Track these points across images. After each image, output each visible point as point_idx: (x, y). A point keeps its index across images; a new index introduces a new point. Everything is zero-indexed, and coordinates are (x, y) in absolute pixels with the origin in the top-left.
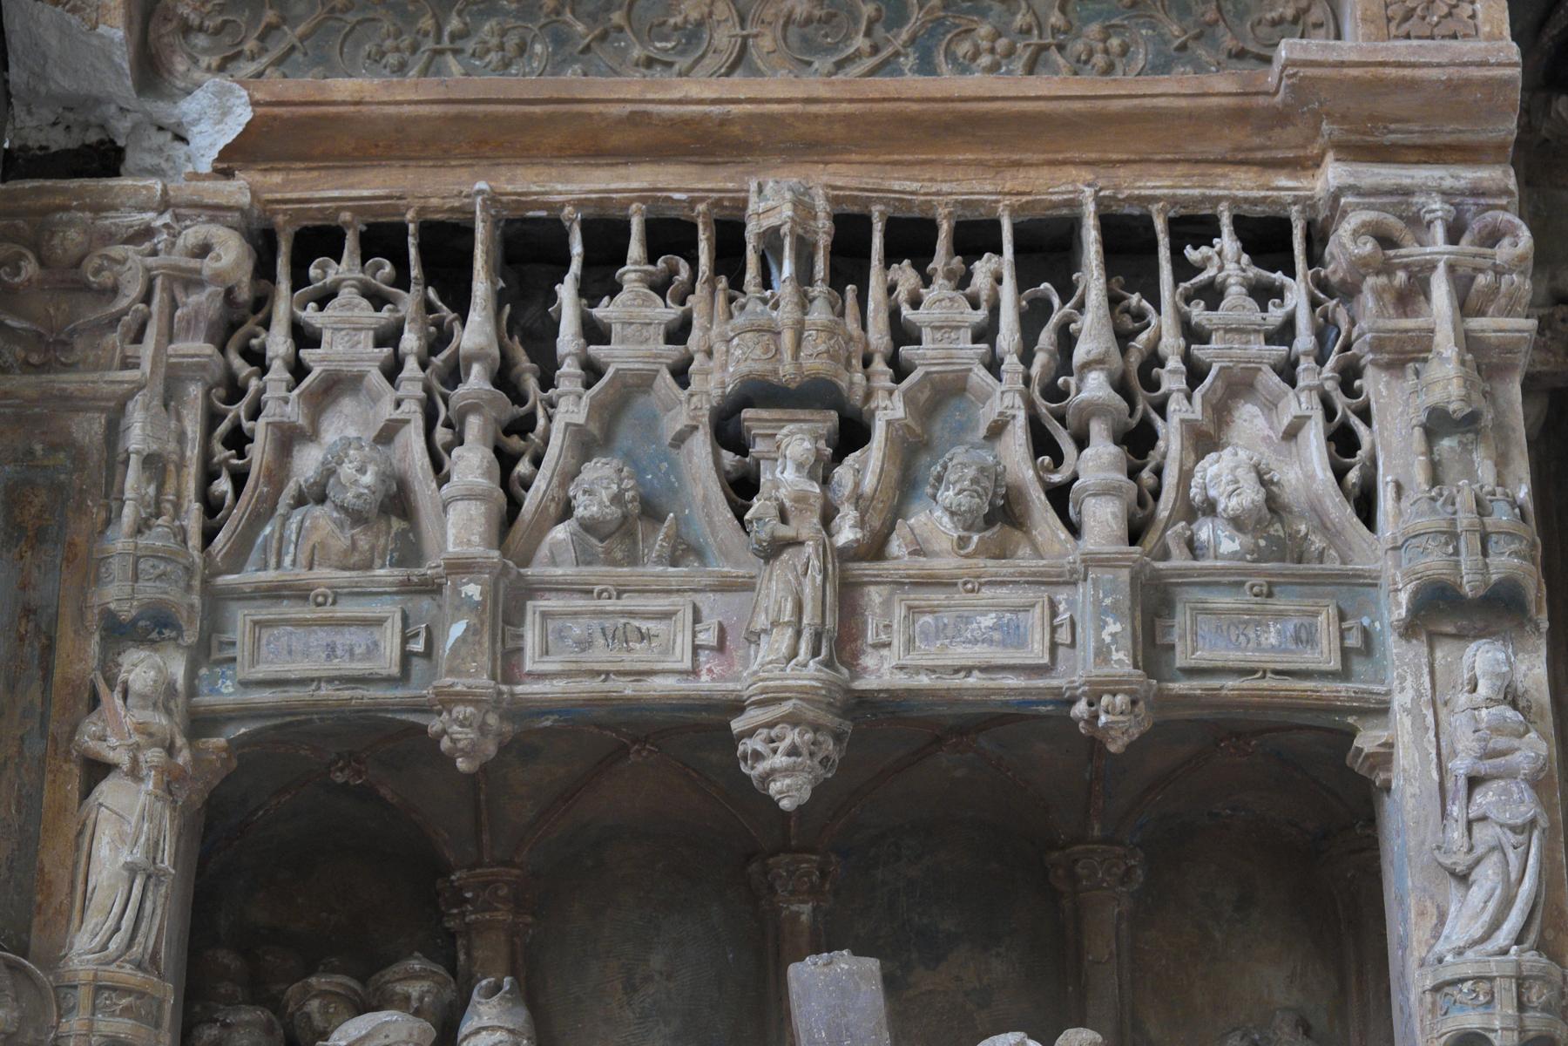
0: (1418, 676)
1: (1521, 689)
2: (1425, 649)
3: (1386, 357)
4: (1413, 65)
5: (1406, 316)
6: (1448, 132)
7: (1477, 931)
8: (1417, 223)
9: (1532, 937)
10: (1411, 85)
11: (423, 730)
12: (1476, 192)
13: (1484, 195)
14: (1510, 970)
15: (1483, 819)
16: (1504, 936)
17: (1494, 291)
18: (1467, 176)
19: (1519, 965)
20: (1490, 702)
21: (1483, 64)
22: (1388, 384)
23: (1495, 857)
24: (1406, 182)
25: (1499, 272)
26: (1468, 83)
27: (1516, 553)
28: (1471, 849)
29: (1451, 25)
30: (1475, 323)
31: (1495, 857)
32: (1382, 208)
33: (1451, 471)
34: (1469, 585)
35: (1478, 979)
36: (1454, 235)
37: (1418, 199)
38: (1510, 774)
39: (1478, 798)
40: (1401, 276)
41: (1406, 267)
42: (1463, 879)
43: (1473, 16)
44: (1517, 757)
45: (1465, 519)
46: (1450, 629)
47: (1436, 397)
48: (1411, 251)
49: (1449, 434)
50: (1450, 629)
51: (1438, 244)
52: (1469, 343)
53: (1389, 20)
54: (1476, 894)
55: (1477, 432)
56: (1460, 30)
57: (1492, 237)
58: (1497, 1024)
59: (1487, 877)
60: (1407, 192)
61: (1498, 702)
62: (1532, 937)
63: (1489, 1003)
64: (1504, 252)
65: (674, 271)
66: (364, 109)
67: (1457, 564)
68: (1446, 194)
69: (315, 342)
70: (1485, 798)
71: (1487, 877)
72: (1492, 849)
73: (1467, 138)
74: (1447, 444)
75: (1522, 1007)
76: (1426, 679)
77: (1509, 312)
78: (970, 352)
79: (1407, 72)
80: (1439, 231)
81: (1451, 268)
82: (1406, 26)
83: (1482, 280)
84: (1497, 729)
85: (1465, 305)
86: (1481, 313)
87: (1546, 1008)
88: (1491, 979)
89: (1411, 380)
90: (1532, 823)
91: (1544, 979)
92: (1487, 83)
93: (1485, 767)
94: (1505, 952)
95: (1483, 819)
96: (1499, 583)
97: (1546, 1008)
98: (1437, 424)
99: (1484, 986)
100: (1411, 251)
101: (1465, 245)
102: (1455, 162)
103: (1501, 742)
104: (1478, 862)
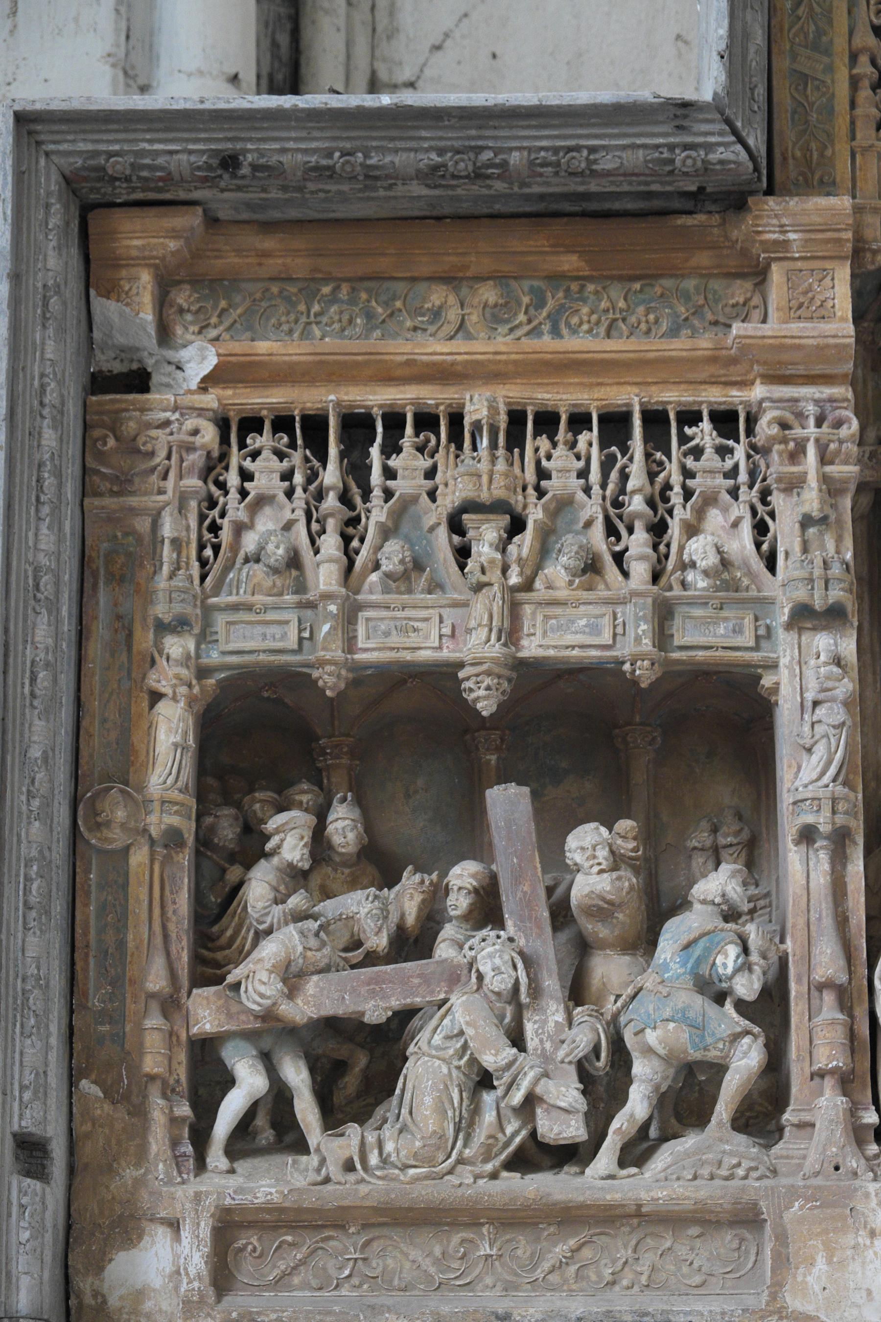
0: (792, 649)
1: (843, 656)
2: (796, 636)
3: (783, 486)
4: (800, 337)
5: (794, 464)
6: (818, 369)
7: (814, 776)
8: (800, 416)
9: (841, 779)
10: (799, 347)
11: (310, 675)
12: (831, 400)
13: (835, 401)
14: (829, 795)
15: (820, 722)
16: (827, 779)
17: (838, 452)
18: (827, 391)
19: (833, 792)
20: (826, 664)
21: (835, 336)
22: (784, 500)
23: (824, 741)
24: (796, 395)
25: (841, 442)
26: (827, 346)
27: (842, 589)
28: (813, 736)
29: (823, 312)
30: (828, 469)
31: (824, 741)
32: (783, 409)
33: (814, 545)
34: (818, 604)
35: (813, 799)
36: (819, 423)
37: (802, 404)
38: (833, 700)
39: (817, 711)
40: (792, 445)
41: (794, 440)
42: (809, 750)
43: (833, 307)
44: (837, 691)
45: (818, 572)
46: (809, 626)
47: (806, 508)
48: (798, 432)
49: (813, 526)
50: (809, 626)
51: (811, 429)
52: (825, 479)
53: (790, 309)
54: (815, 758)
55: (827, 525)
56: (826, 314)
57: (838, 424)
58: (822, 821)
59: (820, 750)
60: (797, 400)
61: (830, 664)
62: (841, 779)
63: (818, 811)
64: (844, 432)
65: (428, 441)
66: (274, 358)
67: (813, 595)
68: (817, 402)
69: (548, 477)
70: (821, 712)
71: (820, 750)
72: (823, 737)
73: (828, 371)
74: (812, 531)
75: (834, 812)
76: (796, 651)
77: (846, 463)
78: (576, 484)
79: (797, 341)
80: (812, 421)
81: (817, 441)
82: (799, 313)
83: (832, 446)
84: (828, 678)
85: (824, 459)
86: (832, 463)
87: (846, 813)
88: (820, 799)
89: (795, 498)
90: (843, 723)
91: (846, 799)
92: (836, 346)
93: (821, 696)
94: (827, 786)
95: (820, 722)
96: (833, 604)
97: (846, 813)
98: (806, 522)
99: (816, 802)
100: (798, 432)
101: (825, 428)
102: (822, 384)
103: (830, 684)
104: (816, 743)
